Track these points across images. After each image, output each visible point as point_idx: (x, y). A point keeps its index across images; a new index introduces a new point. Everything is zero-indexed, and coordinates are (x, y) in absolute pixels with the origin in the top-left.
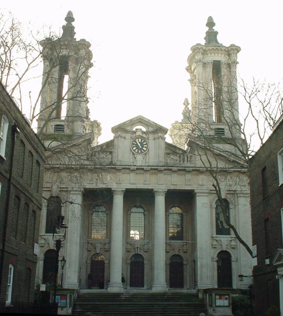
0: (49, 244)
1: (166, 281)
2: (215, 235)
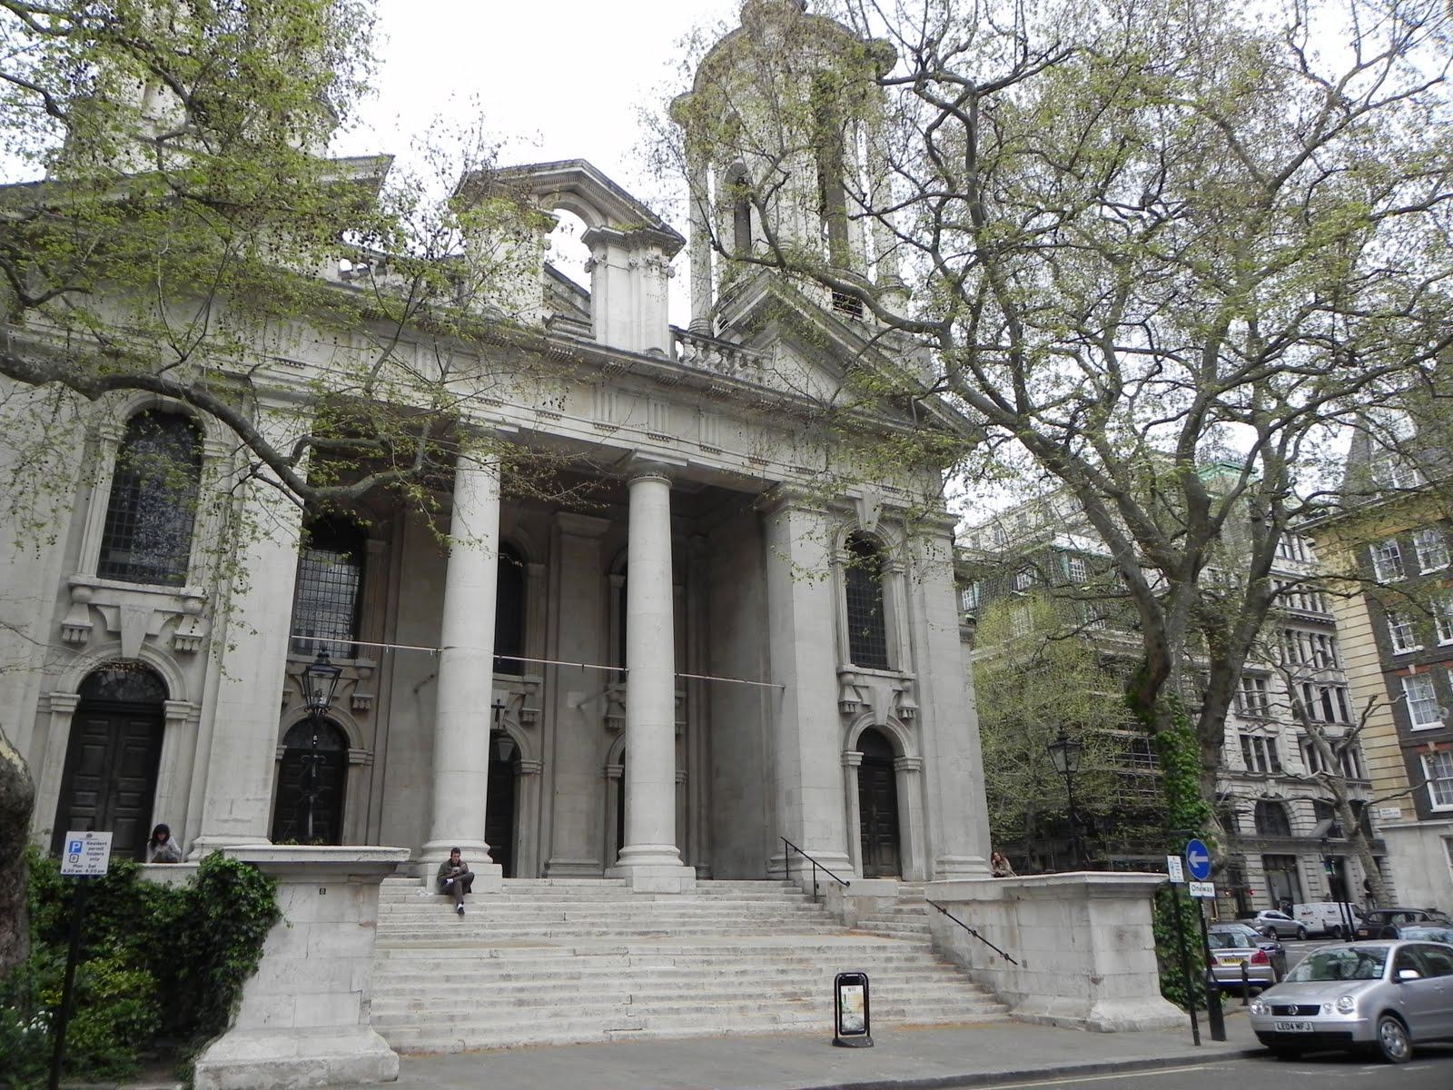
0: (116, 635)
1: (590, 840)
2: (88, 574)
